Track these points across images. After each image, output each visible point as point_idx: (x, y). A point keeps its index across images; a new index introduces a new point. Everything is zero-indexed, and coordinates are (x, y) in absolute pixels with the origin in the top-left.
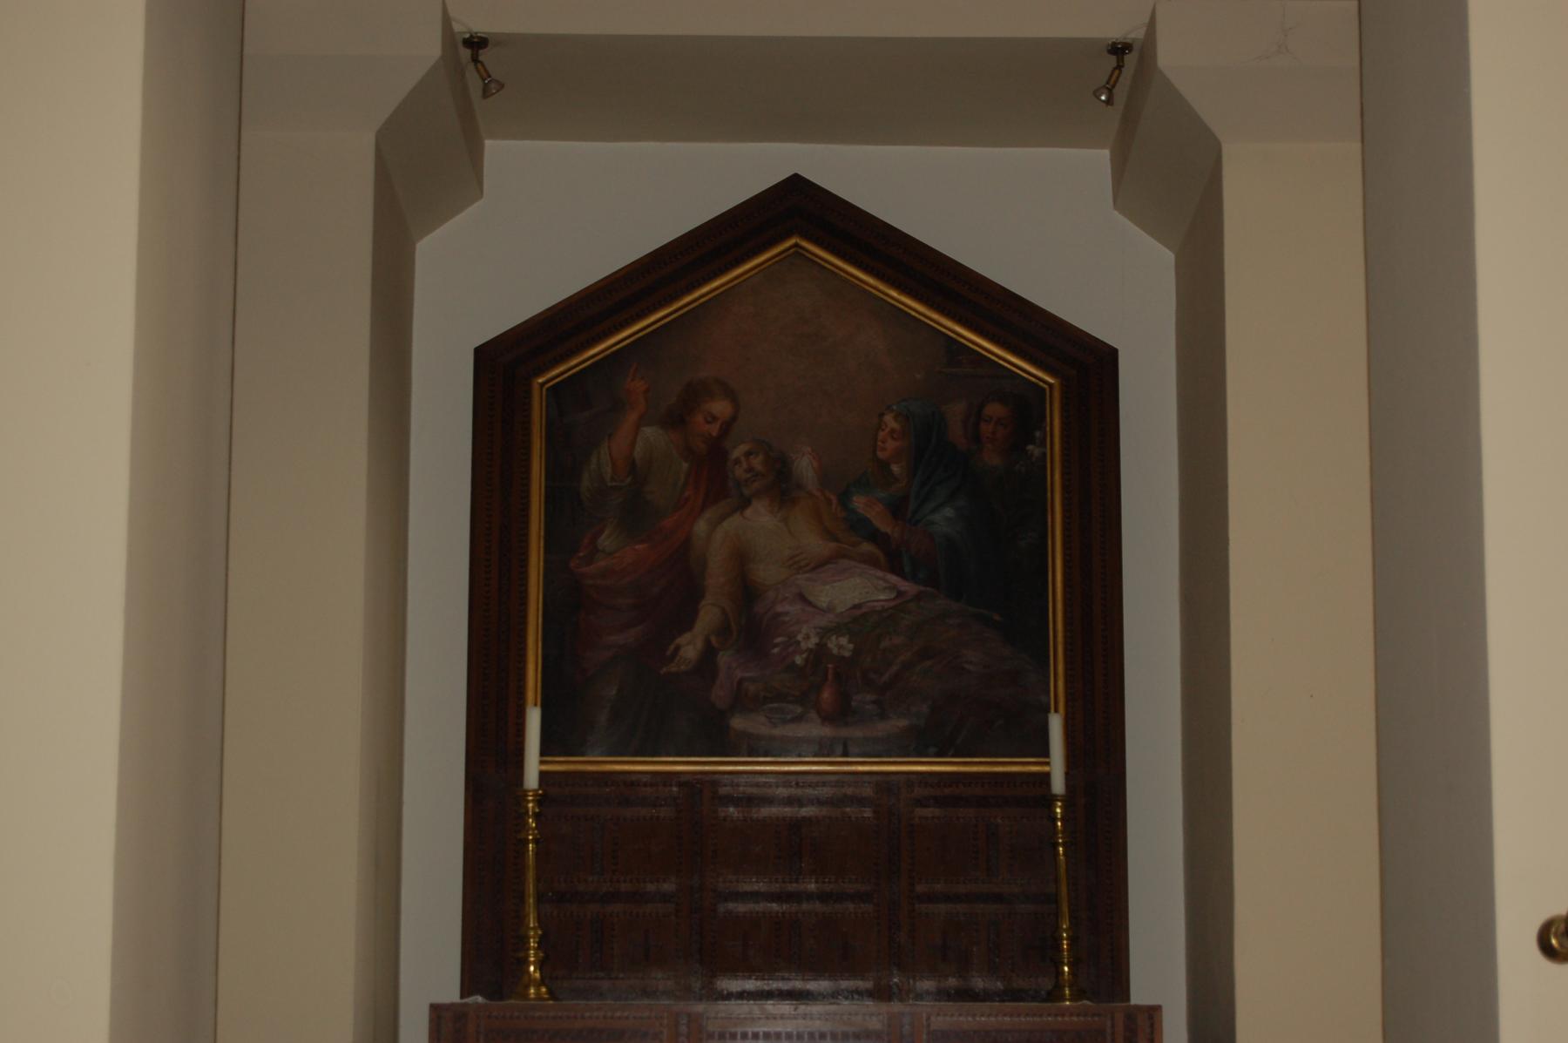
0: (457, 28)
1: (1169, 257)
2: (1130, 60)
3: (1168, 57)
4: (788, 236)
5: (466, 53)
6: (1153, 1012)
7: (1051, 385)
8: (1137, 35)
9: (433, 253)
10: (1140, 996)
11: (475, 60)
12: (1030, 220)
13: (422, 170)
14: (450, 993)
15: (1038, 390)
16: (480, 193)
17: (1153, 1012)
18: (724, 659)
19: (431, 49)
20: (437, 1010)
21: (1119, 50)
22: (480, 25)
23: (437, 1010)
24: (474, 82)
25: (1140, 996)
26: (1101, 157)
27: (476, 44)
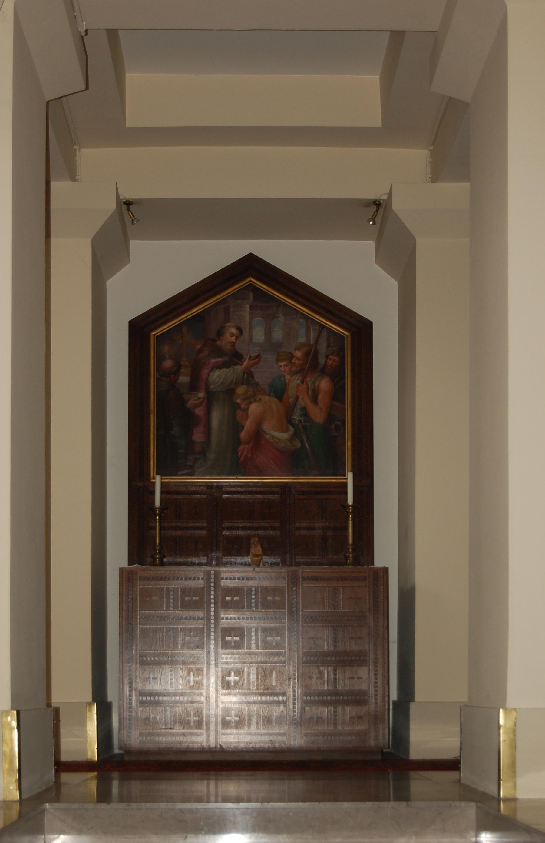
0: (121, 197)
1: (396, 283)
2: (381, 210)
3: (396, 206)
4: (247, 277)
5: (124, 207)
6: (385, 570)
7: (347, 335)
8: (385, 197)
9: (112, 284)
10: (379, 562)
11: (128, 210)
12: (341, 270)
13: (108, 255)
14: (124, 563)
15: (342, 338)
16: (128, 261)
17: (385, 570)
18: (307, 709)
19: (112, 206)
20: (121, 570)
21: (377, 204)
22: (127, 194)
23: (121, 570)
24: (128, 220)
25: (379, 562)
26: (371, 244)
27: (128, 204)
